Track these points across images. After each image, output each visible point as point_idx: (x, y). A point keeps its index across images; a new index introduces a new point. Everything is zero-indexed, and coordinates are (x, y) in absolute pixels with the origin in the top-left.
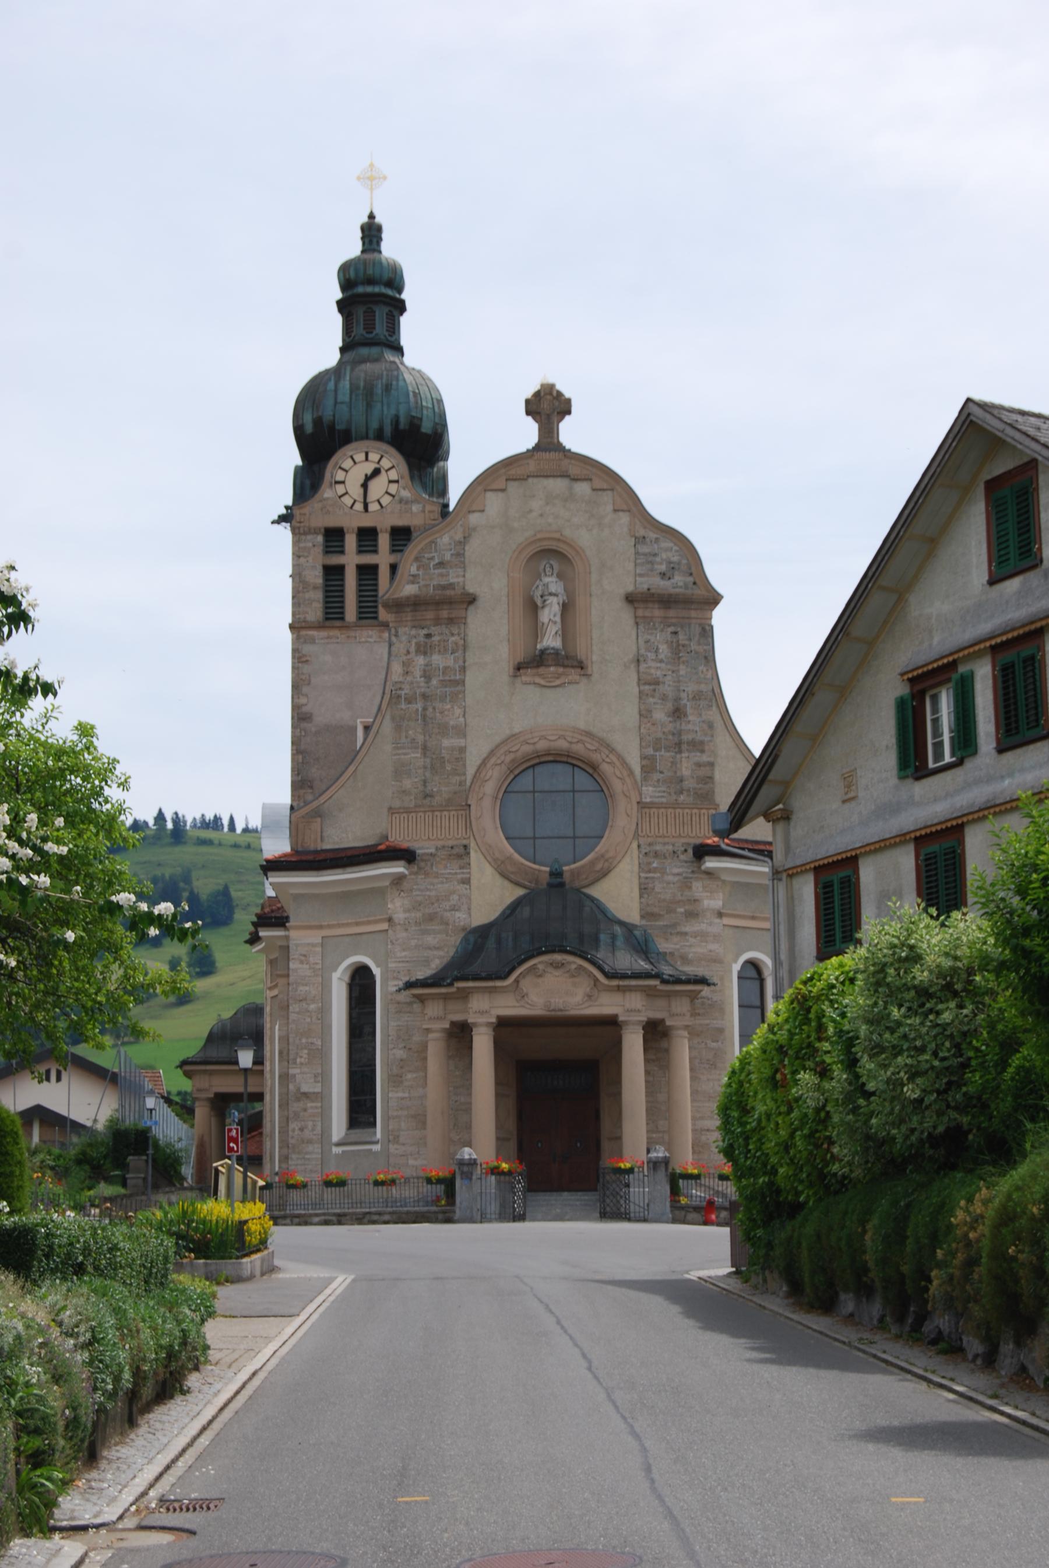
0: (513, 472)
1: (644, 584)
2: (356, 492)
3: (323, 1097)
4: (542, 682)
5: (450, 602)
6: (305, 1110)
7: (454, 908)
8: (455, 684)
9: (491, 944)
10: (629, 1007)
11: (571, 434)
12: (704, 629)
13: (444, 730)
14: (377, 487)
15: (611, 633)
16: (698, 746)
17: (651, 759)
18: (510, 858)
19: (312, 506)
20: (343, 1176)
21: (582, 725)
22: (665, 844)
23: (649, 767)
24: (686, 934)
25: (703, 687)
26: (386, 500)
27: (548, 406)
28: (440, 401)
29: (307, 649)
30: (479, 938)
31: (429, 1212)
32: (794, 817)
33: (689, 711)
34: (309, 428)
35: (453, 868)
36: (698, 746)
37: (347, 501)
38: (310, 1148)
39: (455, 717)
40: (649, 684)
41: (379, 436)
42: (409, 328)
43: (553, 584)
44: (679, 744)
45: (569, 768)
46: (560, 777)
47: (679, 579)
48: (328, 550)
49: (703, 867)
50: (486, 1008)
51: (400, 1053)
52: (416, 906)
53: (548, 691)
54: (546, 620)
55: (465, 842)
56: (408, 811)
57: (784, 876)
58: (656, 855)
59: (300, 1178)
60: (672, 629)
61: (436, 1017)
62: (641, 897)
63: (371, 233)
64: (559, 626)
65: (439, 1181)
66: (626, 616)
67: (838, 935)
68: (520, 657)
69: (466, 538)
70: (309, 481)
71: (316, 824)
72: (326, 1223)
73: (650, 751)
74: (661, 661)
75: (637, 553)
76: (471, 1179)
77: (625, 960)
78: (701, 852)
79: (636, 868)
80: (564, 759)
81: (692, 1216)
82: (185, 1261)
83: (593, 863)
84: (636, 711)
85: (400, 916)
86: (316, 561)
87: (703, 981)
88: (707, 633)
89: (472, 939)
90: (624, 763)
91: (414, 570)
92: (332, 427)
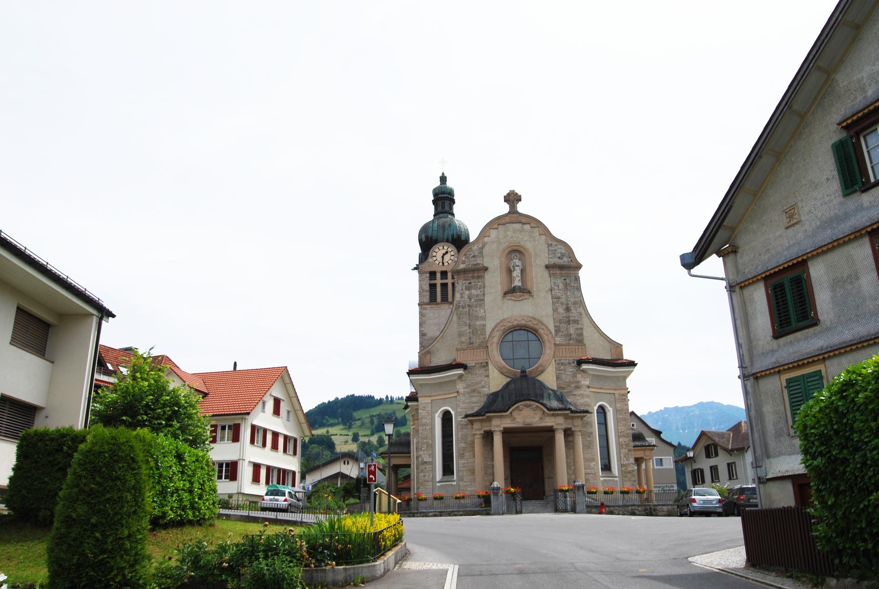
0: (503, 221)
1: (552, 261)
2: (440, 259)
3: (433, 463)
5: (478, 270)
7: (483, 387)
8: (481, 301)
9: (500, 398)
10: (557, 422)
11: (521, 208)
13: (477, 318)
14: (447, 258)
15: (540, 280)
16: (576, 322)
17: (558, 327)
18: (504, 367)
19: (425, 265)
20: (442, 495)
21: (531, 315)
26: (450, 262)
27: (512, 199)
28: (468, 235)
29: (424, 311)
30: (494, 398)
32: (740, 250)
34: (424, 240)
35: (482, 371)
36: (576, 322)
37: (437, 262)
39: (481, 313)
40: (556, 299)
41: (447, 241)
42: (456, 208)
43: (517, 262)
46: (522, 335)
47: (565, 259)
48: (430, 279)
50: (499, 424)
51: (463, 445)
52: (468, 386)
56: (464, 350)
57: (737, 288)
58: (562, 364)
59: (423, 496)
61: (478, 429)
63: (443, 179)
65: (483, 497)
66: (546, 273)
67: (793, 317)
68: (506, 289)
69: (483, 247)
70: (424, 256)
71: (428, 357)
72: (435, 516)
77: (555, 404)
78: (580, 362)
81: (594, 510)
82: (328, 567)
83: (537, 368)
85: (461, 391)
86: (427, 282)
87: (587, 412)
88: (577, 279)
90: (548, 329)
92: (431, 238)
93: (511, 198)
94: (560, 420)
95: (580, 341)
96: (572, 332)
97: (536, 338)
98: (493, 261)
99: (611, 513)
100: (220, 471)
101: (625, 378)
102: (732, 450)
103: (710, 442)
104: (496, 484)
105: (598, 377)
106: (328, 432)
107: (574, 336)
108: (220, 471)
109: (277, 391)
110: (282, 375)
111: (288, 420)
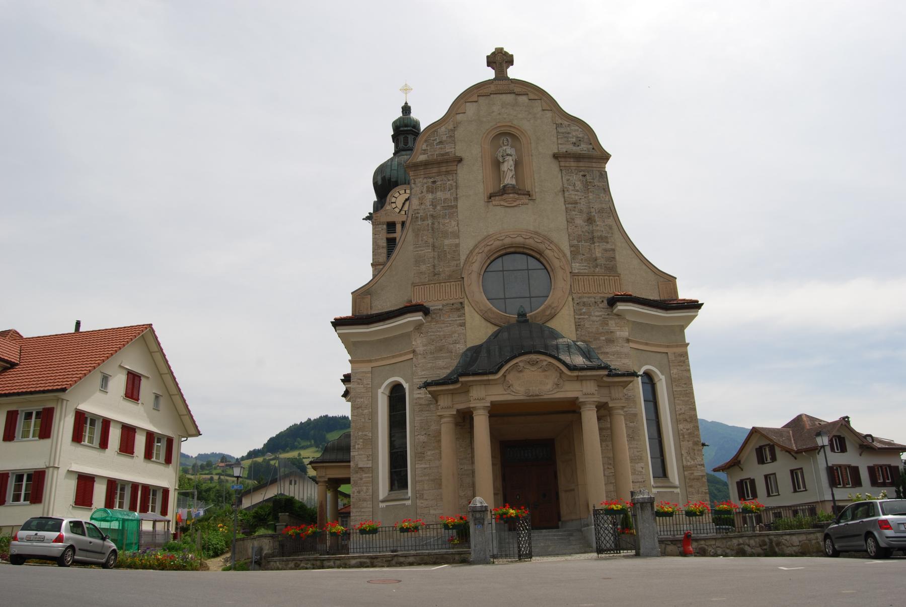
1: (563, 149)
3: (373, 470)
4: (506, 204)
5: (447, 162)
6: (361, 479)
7: (455, 342)
8: (451, 208)
9: (484, 354)
10: (583, 391)
11: (512, 73)
12: (601, 174)
13: (445, 235)
15: (545, 176)
17: (576, 246)
18: (490, 309)
19: (382, 212)
21: (532, 228)
22: (589, 297)
23: (575, 252)
24: (607, 353)
25: (604, 206)
31: (447, 554)
33: (597, 219)
34: (380, 182)
38: (365, 504)
39: (452, 226)
44: (593, 238)
45: (524, 257)
46: (520, 261)
49: (615, 311)
50: (482, 396)
53: (507, 209)
54: (506, 169)
55: (461, 300)
58: (584, 304)
60: (582, 173)
61: (448, 406)
62: (577, 330)
63: (406, 109)
64: (514, 172)
66: (554, 166)
68: (491, 191)
70: (379, 205)
71: (367, 300)
72: (361, 565)
73: (575, 242)
74: (577, 191)
75: (558, 132)
76: (483, 524)
78: (612, 302)
79: (572, 313)
80: (521, 250)
81: (670, 548)
83: (544, 311)
84: (565, 219)
85: (420, 349)
86: (384, 235)
88: (603, 176)
89: (469, 354)
90: (559, 249)
91: (424, 147)
92: (390, 180)
93: (498, 58)
94: (590, 387)
95: (611, 269)
96: (598, 255)
97: (541, 267)
98: (472, 149)
99: (702, 553)
100: (18, 488)
101: (682, 328)
102: (799, 452)
103: (763, 442)
104: (478, 501)
105: (639, 327)
106: (299, 455)
107: (601, 261)
108: (18, 488)
109: (132, 360)
110: (144, 336)
111: (156, 408)
